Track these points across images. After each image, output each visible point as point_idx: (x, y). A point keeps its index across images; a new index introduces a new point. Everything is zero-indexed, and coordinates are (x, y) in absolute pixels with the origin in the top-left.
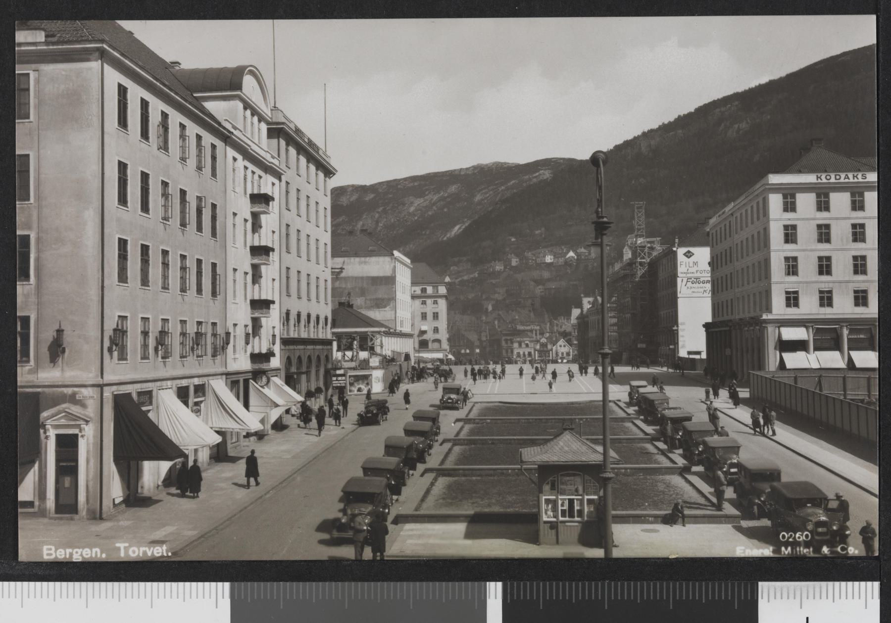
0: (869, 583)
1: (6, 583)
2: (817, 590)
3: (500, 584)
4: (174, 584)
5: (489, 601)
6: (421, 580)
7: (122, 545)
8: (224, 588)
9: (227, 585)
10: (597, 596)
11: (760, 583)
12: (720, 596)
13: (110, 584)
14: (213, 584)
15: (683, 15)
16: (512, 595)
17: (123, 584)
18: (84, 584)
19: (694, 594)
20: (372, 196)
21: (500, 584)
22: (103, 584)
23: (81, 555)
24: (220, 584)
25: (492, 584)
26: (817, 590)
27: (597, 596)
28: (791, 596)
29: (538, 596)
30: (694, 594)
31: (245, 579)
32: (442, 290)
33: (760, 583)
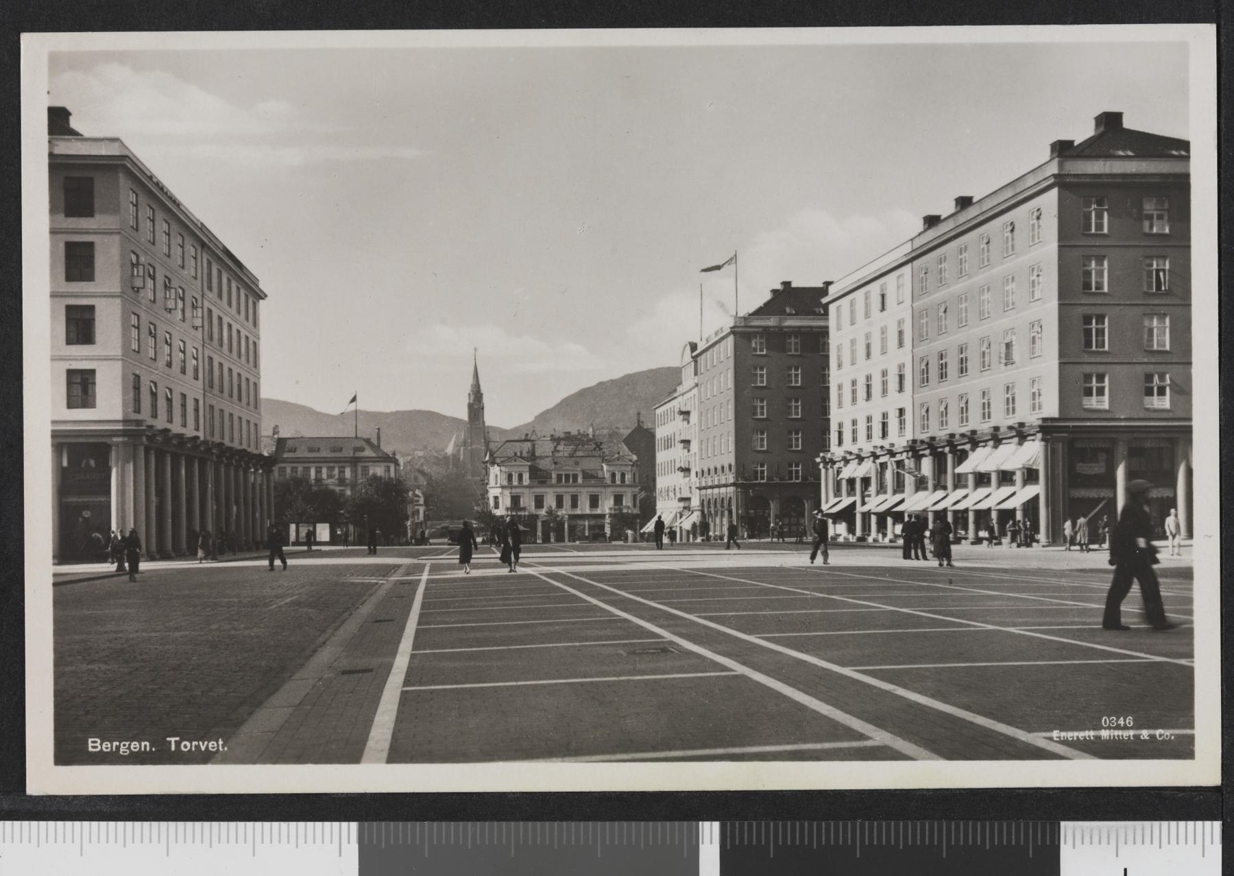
0: (1208, 823)
1: (8, 823)
2: (1139, 833)
3: (716, 825)
4: (284, 825)
5: (701, 846)
6: (612, 819)
7: (173, 740)
9: (354, 825)
10: (845, 839)
11: (1063, 824)
12: (966, 840)
13: (198, 824)
16: (733, 838)
18: (164, 824)
19: (1018, 839)
21: (716, 825)
23: (129, 748)
24: (345, 824)
25: (707, 824)
26: (1139, 833)
27: (845, 839)
28: (1104, 840)
29: (940, 841)
30: (1018, 839)
33: (1063, 824)
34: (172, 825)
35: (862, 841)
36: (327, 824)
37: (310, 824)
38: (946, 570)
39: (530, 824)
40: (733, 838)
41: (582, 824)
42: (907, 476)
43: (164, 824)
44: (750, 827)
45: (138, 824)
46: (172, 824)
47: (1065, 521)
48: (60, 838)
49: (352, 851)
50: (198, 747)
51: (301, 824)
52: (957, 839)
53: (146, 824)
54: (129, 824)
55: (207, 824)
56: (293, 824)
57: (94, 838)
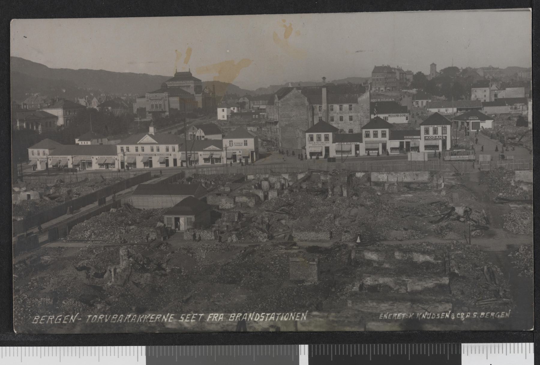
0: (528, 344)
1: (4, 348)
3: (307, 346)
4: (112, 347)
6: (259, 344)
8: (143, 349)
9: (144, 347)
11: (462, 344)
12: (419, 352)
13: (74, 348)
14: (136, 347)
15: (326, 12)
16: (314, 353)
17: (81, 347)
19: (442, 351)
20: (241, 146)
21: (307, 346)
22: (70, 348)
24: (140, 347)
25: (302, 346)
28: (481, 351)
30: (442, 351)
31: (154, 344)
32: (19, 165)
33: (462, 344)
34: (78, 348)
35: (372, 352)
36: (132, 347)
37: (124, 347)
38: (167, 168)
39: (223, 346)
40: (314, 353)
41: (246, 346)
42: (368, 93)
43: (85, 348)
44: (322, 347)
45: (47, 348)
46: (62, 348)
47: (317, 124)
48: (128, 354)
49: (143, 359)
50: (401, 316)
51: (120, 347)
52: (454, 352)
53: (50, 348)
54: (43, 348)
55: (78, 347)
56: (116, 347)
57: (66, 354)
